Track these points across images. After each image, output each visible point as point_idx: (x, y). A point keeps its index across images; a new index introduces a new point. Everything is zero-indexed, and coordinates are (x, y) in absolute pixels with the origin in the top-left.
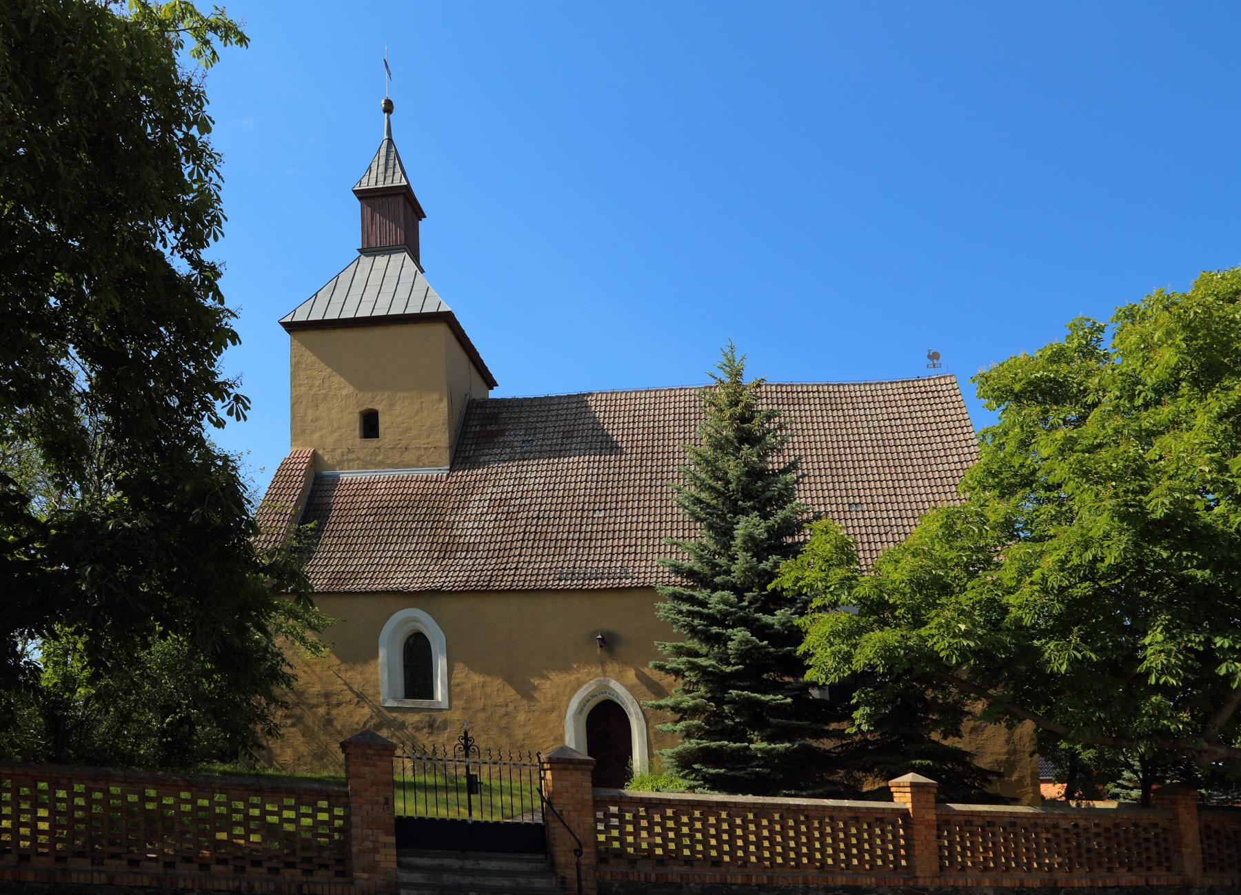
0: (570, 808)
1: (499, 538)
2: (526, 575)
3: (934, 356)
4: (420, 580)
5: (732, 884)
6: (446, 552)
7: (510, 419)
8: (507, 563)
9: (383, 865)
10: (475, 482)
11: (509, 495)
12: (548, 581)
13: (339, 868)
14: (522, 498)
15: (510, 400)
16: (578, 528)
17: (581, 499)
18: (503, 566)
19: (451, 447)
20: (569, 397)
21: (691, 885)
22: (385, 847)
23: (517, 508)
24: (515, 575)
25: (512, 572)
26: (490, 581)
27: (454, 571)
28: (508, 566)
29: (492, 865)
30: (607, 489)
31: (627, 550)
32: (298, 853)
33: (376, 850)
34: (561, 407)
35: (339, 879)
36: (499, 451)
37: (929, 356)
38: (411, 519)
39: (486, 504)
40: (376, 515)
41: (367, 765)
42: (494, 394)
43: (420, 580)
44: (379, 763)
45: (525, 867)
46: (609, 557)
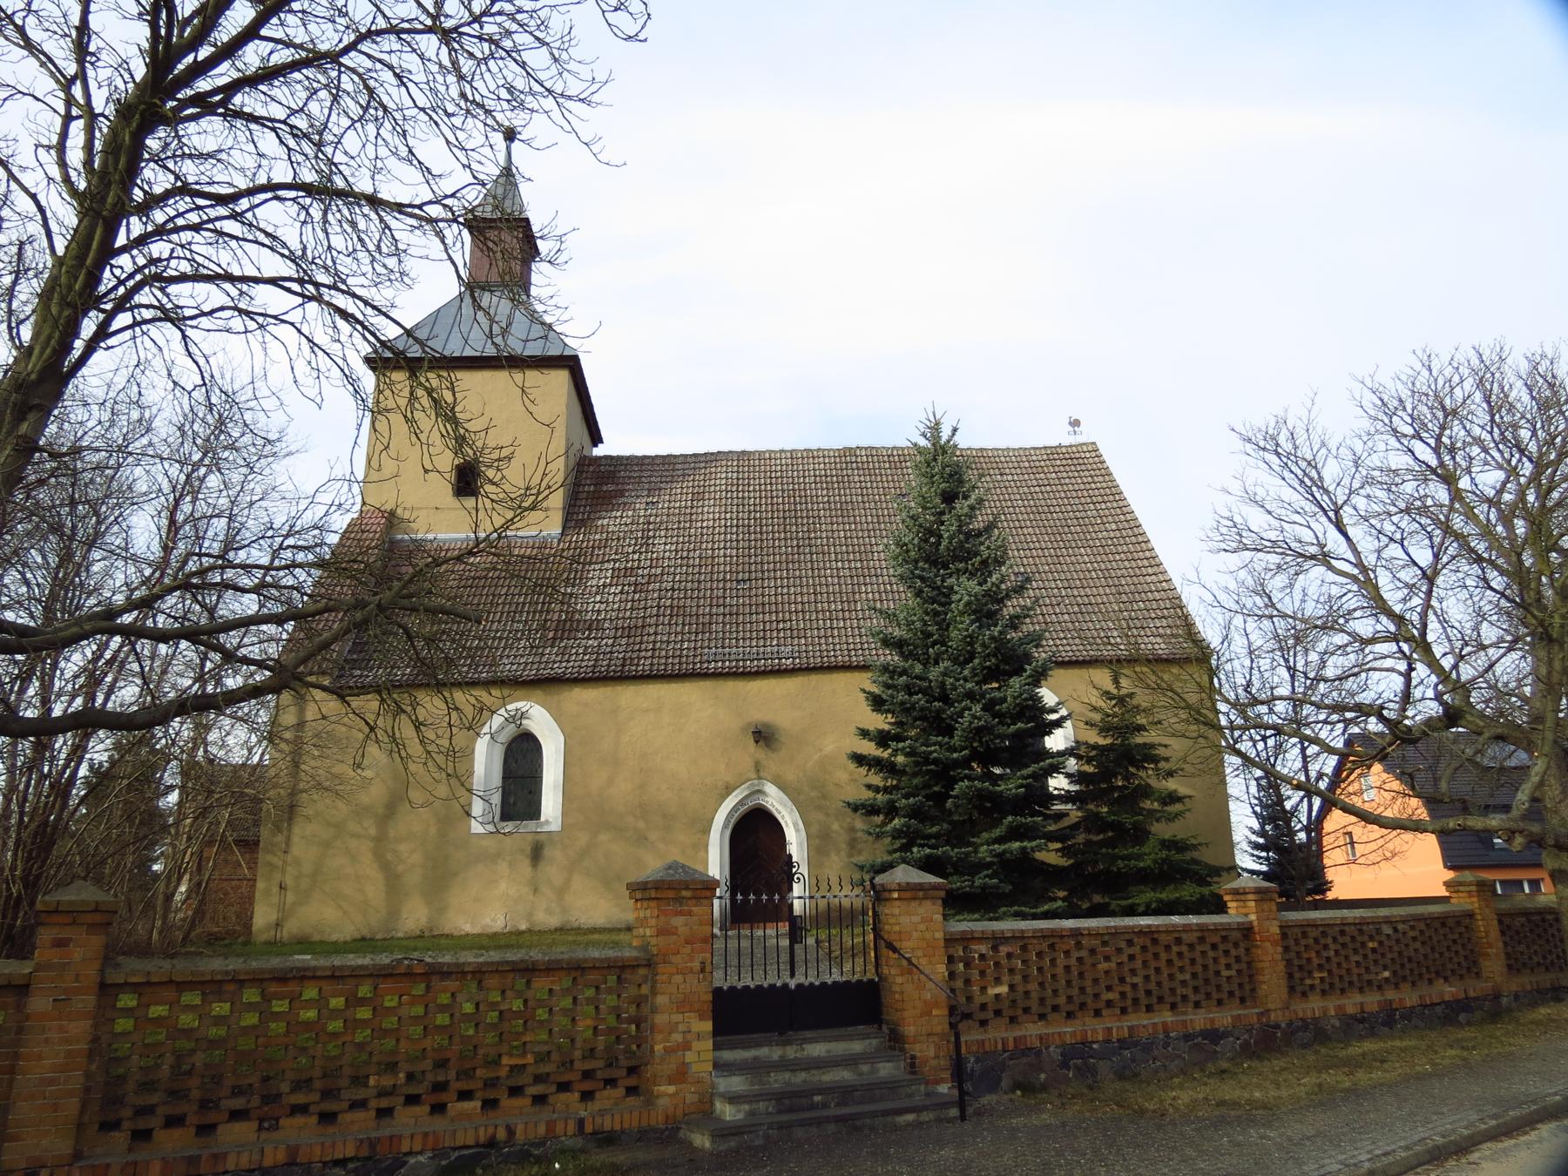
0: (920, 953)
1: (628, 613)
2: (667, 658)
3: (1075, 423)
4: (536, 666)
5: (1093, 1042)
6: (564, 631)
7: (629, 478)
8: (641, 643)
9: (694, 1068)
10: (593, 548)
11: (636, 564)
12: (695, 663)
13: (632, 1082)
14: (651, 567)
15: (628, 458)
16: (721, 601)
17: (722, 568)
18: (637, 647)
19: (564, 508)
20: (695, 455)
21: (1051, 1049)
22: (699, 1039)
23: (646, 578)
24: (652, 657)
25: (650, 654)
26: (623, 665)
27: (577, 654)
28: (643, 646)
29: (817, 1050)
30: (750, 556)
31: (781, 626)
32: (578, 1065)
33: (686, 1046)
34: (687, 466)
35: (631, 1100)
36: (619, 514)
37: (1070, 423)
38: (517, 591)
39: (609, 575)
40: (471, 587)
41: (681, 913)
42: (598, 451)
43: (536, 666)
44: (694, 909)
45: (857, 1047)
46: (762, 634)
